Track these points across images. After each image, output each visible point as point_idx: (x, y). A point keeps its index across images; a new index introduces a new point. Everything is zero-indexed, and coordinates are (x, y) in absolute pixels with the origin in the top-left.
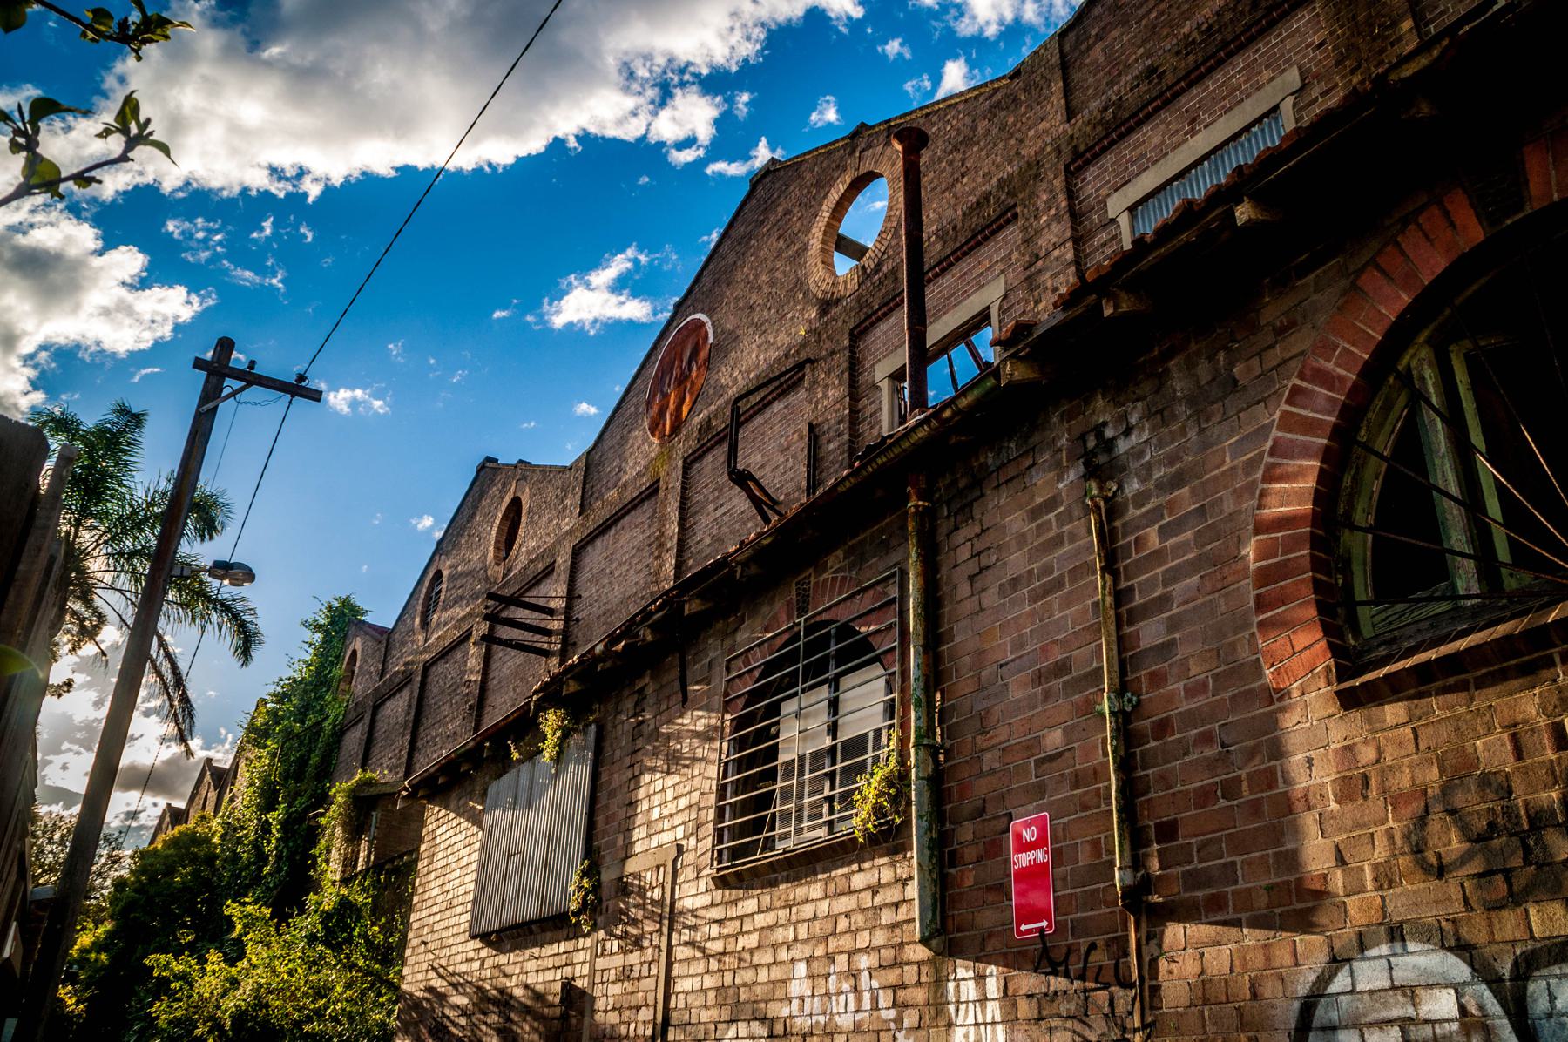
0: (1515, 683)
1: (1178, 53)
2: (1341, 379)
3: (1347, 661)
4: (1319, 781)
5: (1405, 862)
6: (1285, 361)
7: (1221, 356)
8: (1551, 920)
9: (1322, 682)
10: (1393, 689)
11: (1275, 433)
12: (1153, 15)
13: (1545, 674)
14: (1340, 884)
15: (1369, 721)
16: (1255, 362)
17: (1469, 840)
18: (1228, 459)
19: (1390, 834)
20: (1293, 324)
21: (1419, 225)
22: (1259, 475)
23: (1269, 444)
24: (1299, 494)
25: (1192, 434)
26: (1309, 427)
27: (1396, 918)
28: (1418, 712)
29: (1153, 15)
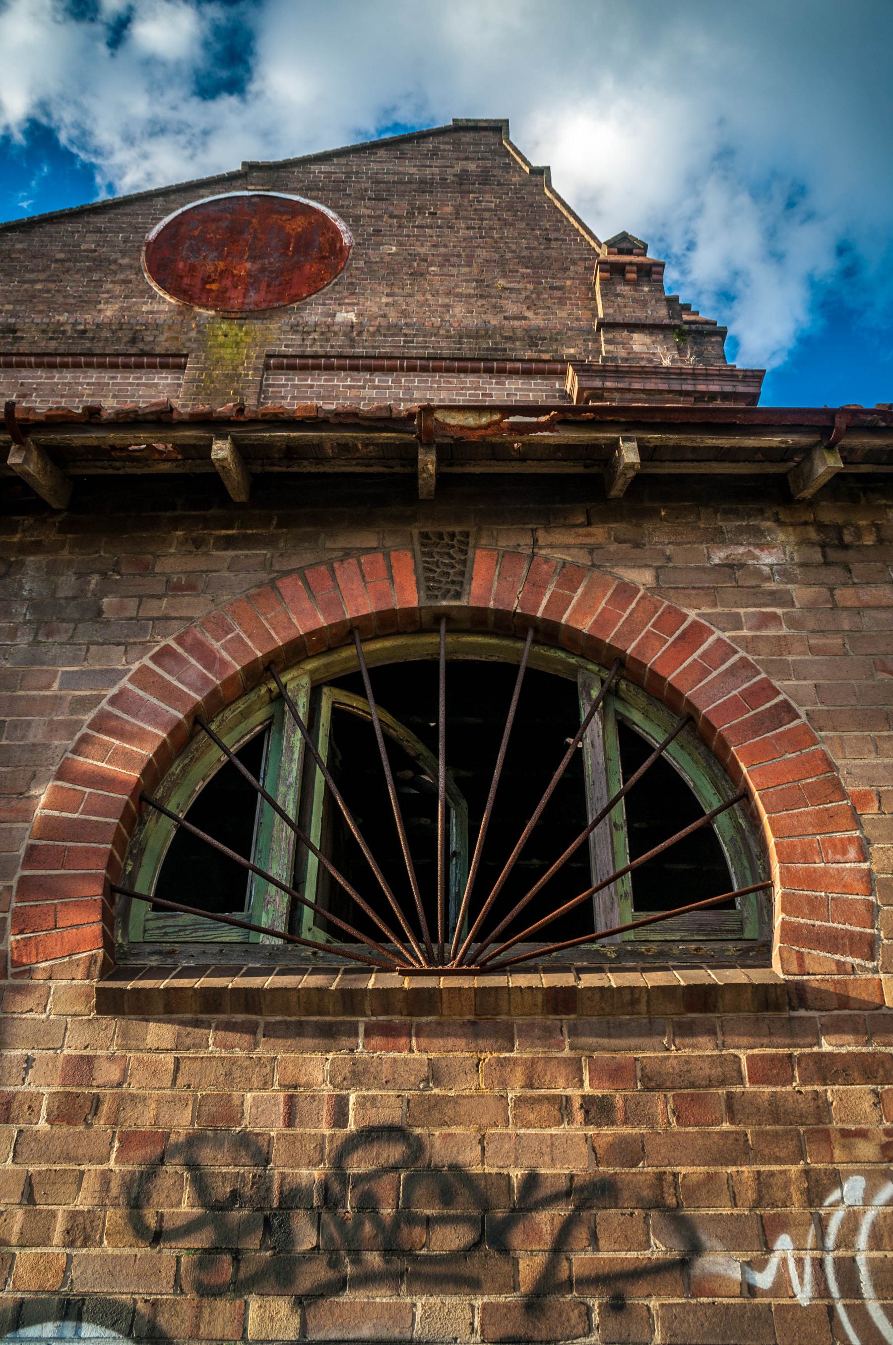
0: (310, 1042)
1: (44, 331)
2: (224, 663)
3: (116, 962)
4: (32, 1089)
5: (114, 1216)
6: (167, 618)
7: (94, 580)
8: (272, 1319)
9: (80, 971)
10: (170, 1006)
11: (125, 682)
12: (39, 286)
13: (345, 1041)
14: (16, 1229)
15: (125, 1035)
16: (133, 603)
17: (204, 1206)
18: (56, 686)
19: (105, 1178)
20: (191, 587)
21: (360, 564)
22: (88, 717)
23: (115, 690)
24: (127, 759)
25: (23, 641)
26: (169, 694)
27: (79, 1288)
28: (188, 1041)
29: (39, 286)
